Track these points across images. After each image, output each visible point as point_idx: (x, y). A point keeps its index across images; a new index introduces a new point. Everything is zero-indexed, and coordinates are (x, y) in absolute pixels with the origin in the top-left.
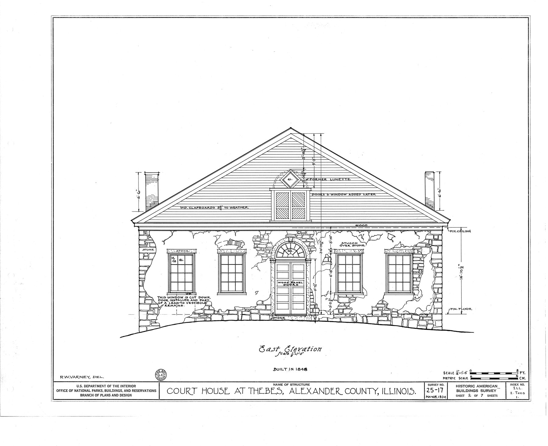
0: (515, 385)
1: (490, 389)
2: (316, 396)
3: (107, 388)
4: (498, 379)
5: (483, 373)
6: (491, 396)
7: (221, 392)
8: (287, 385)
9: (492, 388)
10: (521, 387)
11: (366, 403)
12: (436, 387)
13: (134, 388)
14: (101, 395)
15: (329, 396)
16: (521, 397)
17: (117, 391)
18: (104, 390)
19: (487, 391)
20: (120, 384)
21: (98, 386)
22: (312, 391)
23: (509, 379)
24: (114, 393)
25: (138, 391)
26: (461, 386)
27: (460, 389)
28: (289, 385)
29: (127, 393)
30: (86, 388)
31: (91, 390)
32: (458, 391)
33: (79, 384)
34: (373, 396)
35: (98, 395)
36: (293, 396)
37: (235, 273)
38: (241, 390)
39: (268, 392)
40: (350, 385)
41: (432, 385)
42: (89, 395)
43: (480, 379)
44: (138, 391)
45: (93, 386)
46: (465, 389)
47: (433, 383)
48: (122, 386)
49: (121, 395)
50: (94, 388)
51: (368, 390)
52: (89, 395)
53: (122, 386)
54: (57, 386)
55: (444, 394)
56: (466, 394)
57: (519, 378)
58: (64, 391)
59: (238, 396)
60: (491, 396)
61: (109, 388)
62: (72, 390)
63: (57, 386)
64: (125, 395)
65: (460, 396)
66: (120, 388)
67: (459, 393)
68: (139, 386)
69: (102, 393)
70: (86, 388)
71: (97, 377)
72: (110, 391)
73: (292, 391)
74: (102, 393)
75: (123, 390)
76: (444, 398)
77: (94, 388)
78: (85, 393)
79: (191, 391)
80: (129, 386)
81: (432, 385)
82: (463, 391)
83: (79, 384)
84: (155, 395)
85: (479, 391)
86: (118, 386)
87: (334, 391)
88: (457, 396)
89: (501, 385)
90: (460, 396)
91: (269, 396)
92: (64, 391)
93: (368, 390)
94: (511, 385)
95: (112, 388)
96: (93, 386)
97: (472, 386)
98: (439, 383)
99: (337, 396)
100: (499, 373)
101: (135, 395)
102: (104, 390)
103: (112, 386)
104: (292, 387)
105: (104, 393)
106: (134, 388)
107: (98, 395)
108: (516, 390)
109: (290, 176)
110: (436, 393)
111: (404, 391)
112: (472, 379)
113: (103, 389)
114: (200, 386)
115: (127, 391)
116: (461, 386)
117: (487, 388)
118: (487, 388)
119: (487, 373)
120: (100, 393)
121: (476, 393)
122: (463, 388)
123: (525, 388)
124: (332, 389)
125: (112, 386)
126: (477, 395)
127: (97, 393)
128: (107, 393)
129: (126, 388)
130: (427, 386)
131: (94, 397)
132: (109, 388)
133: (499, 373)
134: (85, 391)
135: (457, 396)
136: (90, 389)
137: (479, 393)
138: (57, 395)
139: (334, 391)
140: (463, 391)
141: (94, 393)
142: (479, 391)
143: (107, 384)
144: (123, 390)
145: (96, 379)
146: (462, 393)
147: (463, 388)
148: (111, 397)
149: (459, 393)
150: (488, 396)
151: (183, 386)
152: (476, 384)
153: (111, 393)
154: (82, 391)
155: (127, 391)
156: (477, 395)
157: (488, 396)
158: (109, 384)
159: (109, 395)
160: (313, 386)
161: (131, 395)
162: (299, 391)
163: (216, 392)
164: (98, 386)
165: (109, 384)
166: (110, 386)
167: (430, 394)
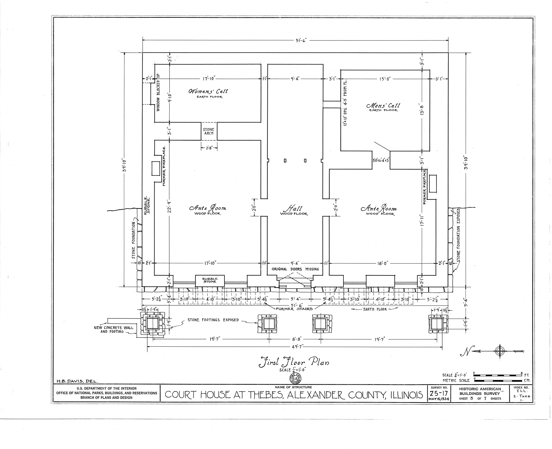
0: (519, 387)
1: (493, 391)
3: (107, 390)
4: (502, 381)
6: (495, 399)
8: (289, 387)
9: (495, 391)
10: (526, 390)
13: (135, 391)
17: (117, 393)
18: (104, 393)
19: (491, 393)
21: (99, 388)
22: (312, 395)
24: (115, 395)
25: (139, 393)
26: (465, 389)
27: (463, 391)
28: (291, 387)
29: (128, 395)
30: (87, 391)
31: (91, 393)
32: (461, 394)
33: (80, 386)
35: (98, 397)
38: (240, 394)
39: (268, 396)
41: (435, 387)
42: (89, 397)
44: (139, 393)
45: (94, 388)
48: (123, 388)
49: (122, 398)
50: (94, 391)
51: (375, 393)
52: (89, 397)
53: (123, 388)
58: (64, 393)
60: (495, 399)
61: (110, 391)
62: (72, 393)
63: (58, 388)
64: (126, 398)
65: (463, 399)
66: (120, 391)
67: (462, 396)
68: (140, 389)
69: (102, 395)
70: (87, 391)
72: (110, 393)
73: (290, 395)
74: (102, 395)
75: (124, 393)
76: (447, 401)
77: (94, 391)
78: (85, 395)
79: (191, 396)
80: (130, 388)
81: (435, 387)
82: (466, 394)
84: (156, 398)
85: (483, 393)
86: (118, 388)
87: (336, 395)
88: (460, 399)
89: (505, 388)
90: (463, 399)
92: (64, 393)
93: (375, 393)
95: (112, 390)
96: (94, 388)
97: (476, 389)
101: (136, 398)
102: (104, 393)
103: (113, 388)
105: (104, 396)
106: (135, 391)
107: (98, 397)
112: (475, 381)
113: (104, 391)
116: (465, 389)
118: (472, 391)
120: (100, 395)
121: (479, 396)
123: (529, 391)
125: (113, 388)
126: (480, 398)
127: (98, 395)
128: (107, 395)
129: (127, 391)
130: (430, 389)
131: (95, 400)
132: (110, 391)
134: (85, 393)
135: (460, 399)
136: (91, 391)
137: (483, 396)
139: (336, 395)
140: (466, 394)
141: (95, 395)
142: (483, 393)
143: (108, 386)
144: (124, 393)
148: (112, 400)
149: (462, 396)
150: (492, 399)
152: (479, 387)
153: (112, 396)
154: (83, 393)
156: (480, 398)
157: (492, 399)
158: (110, 386)
159: (109, 398)
161: (131, 398)
162: (298, 395)
164: (99, 388)
165: (110, 386)
166: (110, 388)
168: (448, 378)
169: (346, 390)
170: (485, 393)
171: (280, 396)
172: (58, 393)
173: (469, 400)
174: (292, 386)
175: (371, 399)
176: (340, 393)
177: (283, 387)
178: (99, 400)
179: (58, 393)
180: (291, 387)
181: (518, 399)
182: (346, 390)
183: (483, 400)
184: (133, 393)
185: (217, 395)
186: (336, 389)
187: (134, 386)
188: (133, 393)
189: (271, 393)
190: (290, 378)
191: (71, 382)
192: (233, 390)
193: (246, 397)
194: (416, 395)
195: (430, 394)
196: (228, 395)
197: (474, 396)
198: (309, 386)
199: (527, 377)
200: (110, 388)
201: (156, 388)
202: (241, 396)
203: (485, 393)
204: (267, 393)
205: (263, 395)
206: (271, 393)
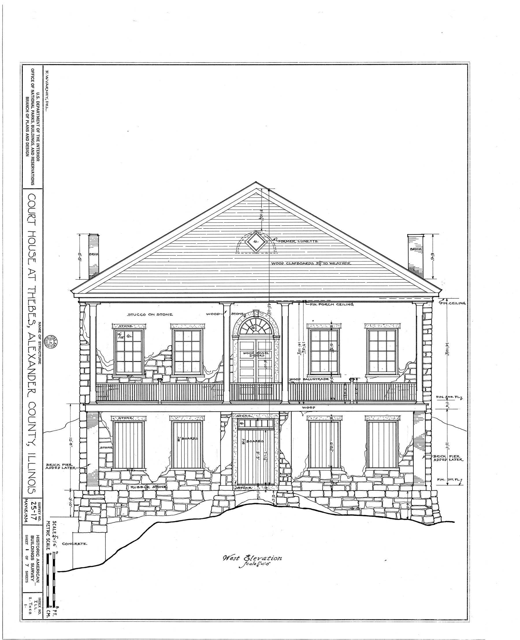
0: (40, 604)
1: (35, 574)
2: (26, 364)
3: (36, 127)
4: (48, 563)
5: (54, 588)
6: (27, 575)
7: (31, 255)
8: (40, 338)
9: (35, 576)
10: (37, 610)
11: (19, 416)
12: (37, 512)
13: (35, 159)
14: (28, 121)
15: (26, 380)
16: (26, 610)
17: (33, 139)
18: (33, 124)
19: (33, 571)
20: (41, 143)
21: (38, 117)
22: (32, 359)
23: (48, 576)
24: (30, 136)
25: (33, 164)
26: (38, 541)
27: (35, 539)
28: (40, 340)
29: (30, 151)
30: (35, 104)
31: (33, 109)
32: (32, 537)
33: (41, 95)
34: (27, 439)
35: (28, 117)
36: (26, 337)
37: (192, 341)
38: (32, 275)
39: (31, 309)
40: (39, 409)
41: (40, 507)
42: (27, 106)
43: (48, 584)
44: (33, 164)
45: (38, 112)
46: (35, 545)
47: (41, 507)
48: (38, 145)
49: (27, 145)
50: (35, 112)
51: (33, 433)
52: (27, 106)
53: (38, 145)
54: (38, 70)
55: (30, 521)
56: (29, 547)
57: (48, 609)
58: (33, 77)
59: (26, 272)
60: (27, 575)
61: (35, 130)
62: (33, 87)
63: (38, 70)
64: (27, 149)
65: (27, 539)
66: (36, 143)
67: (29, 538)
68: (38, 165)
69: (30, 122)
70: (35, 104)
71: (47, 105)
72: (33, 131)
73: (31, 336)
74: (30, 122)
75: (33, 146)
76: (24, 520)
77: (35, 112)
78: (30, 102)
79: (31, 219)
80: (38, 153)
81: (40, 507)
82: (32, 543)
83: (41, 95)
84: (27, 184)
85: (33, 562)
86: (38, 140)
87: (32, 386)
88: (27, 536)
89: (38, 587)
90: (27, 539)
91: (26, 311)
92: (33, 77)
93: (33, 433)
94: (40, 600)
95: (36, 133)
96: (38, 112)
97: (38, 554)
98: (41, 516)
99: (26, 391)
100: (54, 565)
101: (27, 160)
102: (33, 124)
103: (38, 134)
104: (37, 337)
105: (30, 124)
106: (35, 159)
107: (28, 117)
108: (34, 604)
109: (256, 238)
110: (30, 512)
111: (32, 483)
112: (48, 555)
113: (35, 124)
114: (38, 229)
115: (33, 151)
116: (38, 541)
117: (35, 570)
118: (35, 570)
119: (54, 592)
120: (30, 119)
121: (30, 558)
122: (35, 542)
123: (35, 615)
124: (34, 314)
125: (38, 134)
126: (27, 559)
127: (30, 116)
128: (30, 127)
129: (35, 150)
130: (38, 501)
131: (25, 113)
132: (35, 130)
133: (54, 565)
134: (33, 102)
135: (27, 536)
136: (35, 109)
137: (30, 562)
138: (27, 70)
139: (32, 386)
140: (32, 543)
141: (30, 113)
142: (33, 562)
143: (41, 128)
144: (33, 146)
145: (45, 103)
146: (30, 542)
147: (35, 542)
148: (25, 133)
149: (29, 538)
150: (27, 572)
151: (38, 211)
152: (40, 558)
153: (29, 133)
154: (33, 99)
155: (33, 151)
156: (27, 559)
157: (27, 572)
158: (41, 131)
159: (27, 130)
160: (38, 367)
161: (27, 155)
162: (31, 344)
163: (31, 248)
164: (38, 117)
165: (41, 131)
166: (38, 131)
167: (29, 506)
168: (51, 527)
169: (36, 397)
170: (33, 565)
171: (31, 322)
172: (33, 71)
173: (25, 547)
174: (41, 341)
175: (26, 427)
176: (34, 391)
177: (40, 331)
178: (25, 119)
179: (33, 71)
180: (40, 340)
181: (26, 601)
182: (36, 397)
183: (25, 562)
184: (33, 158)
185: (31, 248)
186: (38, 387)
187: (41, 158)
188: (33, 158)
189: (34, 312)
190: (52, 336)
191: (45, 87)
192: (37, 266)
193: (29, 283)
194: (32, 486)
195: (34, 501)
196: (31, 261)
197: (30, 552)
198: (41, 361)
199: (52, 613)
200: (38, 131)
201: (38, 184)
202: (31, 276)
203: (33, 565)
204: (34, 308)
205: (32, 303)
206: (34, 312)
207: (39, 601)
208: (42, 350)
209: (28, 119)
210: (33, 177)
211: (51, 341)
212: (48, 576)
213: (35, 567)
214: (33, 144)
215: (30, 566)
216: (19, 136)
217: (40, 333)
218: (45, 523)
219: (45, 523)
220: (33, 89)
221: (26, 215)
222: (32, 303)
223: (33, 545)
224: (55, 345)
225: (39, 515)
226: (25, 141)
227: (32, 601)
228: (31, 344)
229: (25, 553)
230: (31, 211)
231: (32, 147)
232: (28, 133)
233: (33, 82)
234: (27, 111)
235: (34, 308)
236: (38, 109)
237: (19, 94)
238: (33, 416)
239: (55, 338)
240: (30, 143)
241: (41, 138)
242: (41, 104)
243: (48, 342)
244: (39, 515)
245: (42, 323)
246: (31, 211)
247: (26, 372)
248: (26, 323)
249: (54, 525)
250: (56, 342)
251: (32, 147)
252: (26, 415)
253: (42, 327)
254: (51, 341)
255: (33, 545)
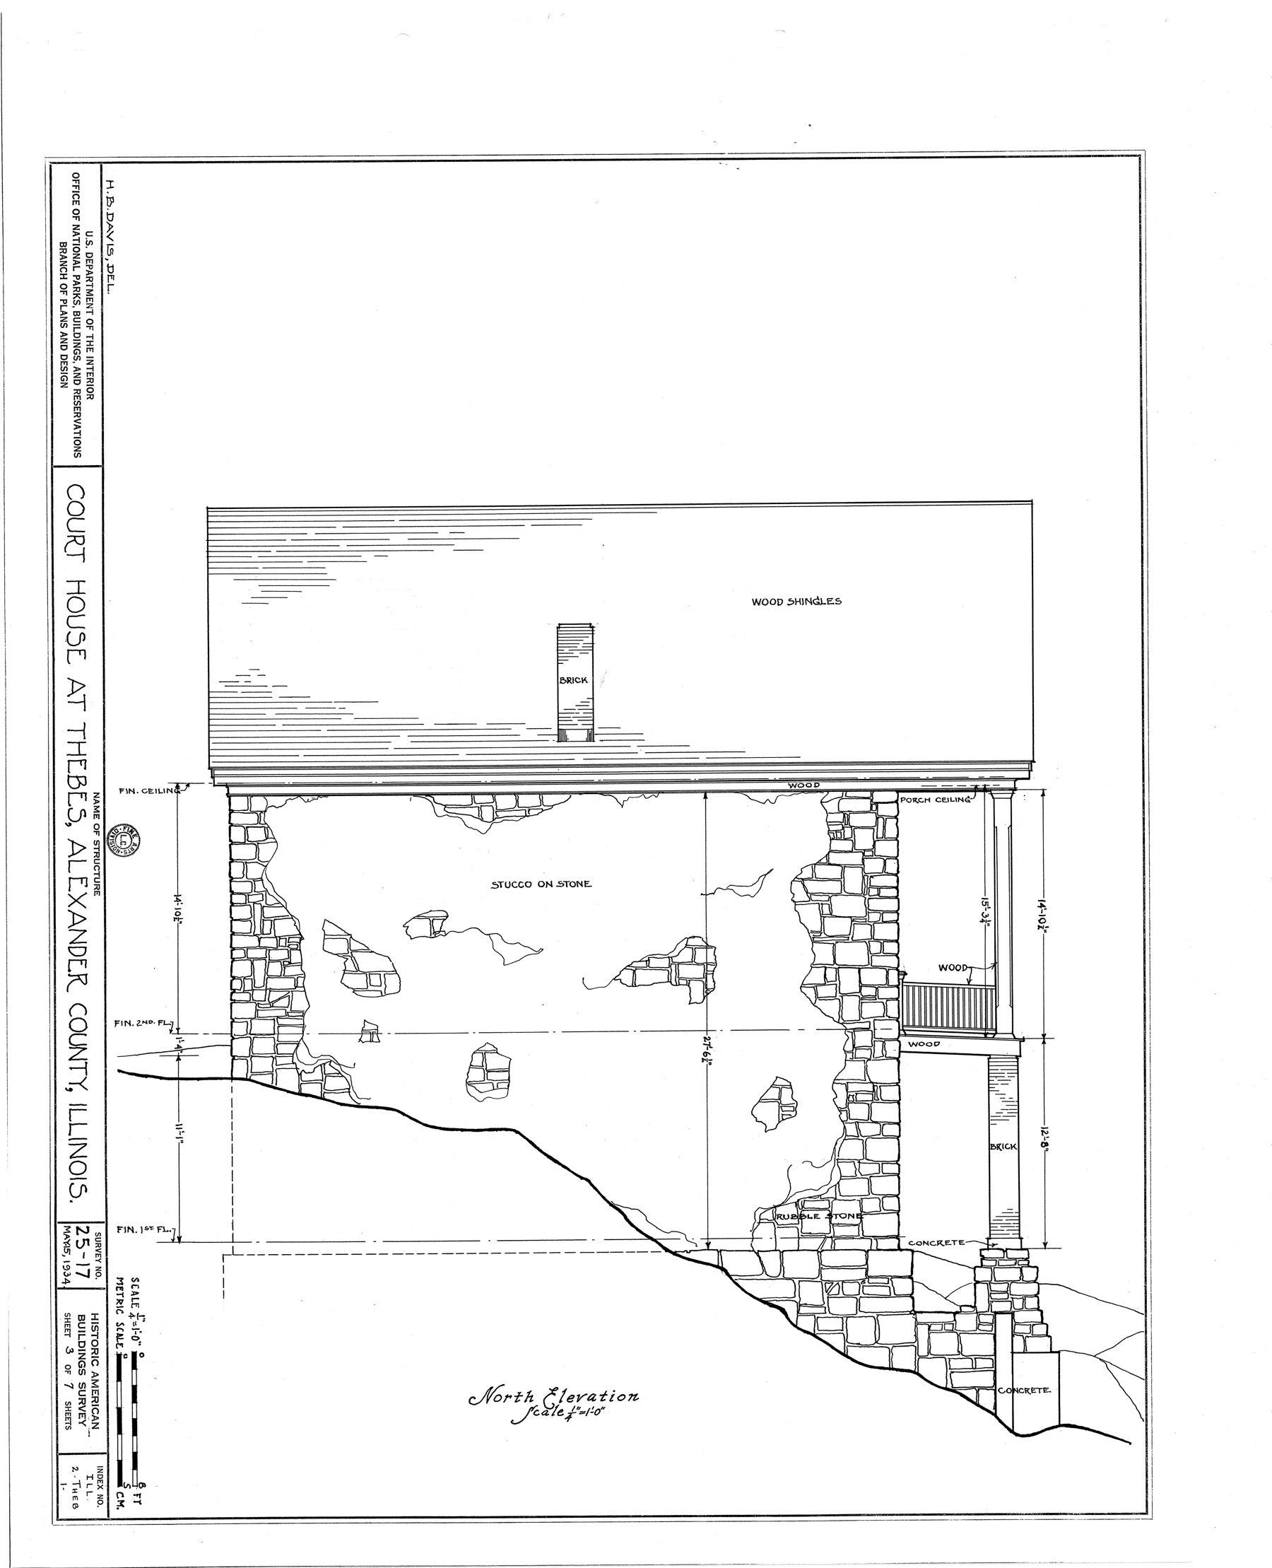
1: (88, 1408)
3: (84, 317)
4: (120, 1431)
5: (134, 1388)
6: (68, 1413)
8: (97, 832)
9: (89, 1414)
10: (93, 1498)
11: (46, 1057)
13: (84, 394)
14: (65, 301)
16: (66, 1495)
17: (77, 346)
18: (77, 308)
19: (83, 1401)
21: (89, 292)
23: (120, 1463)
24: (70, 338)
25: (77, 406)
26: (95, 1328)
27: (88, 1324)
28: (96, 838)
29: (71, 375)
30: (83, 258)
31: (77, 271)
32: (82, 1318)
33: (96, 239)
35: (64, 291)
36: (64, 850)
38: (78, 697)
41: (99, 1245)
42: (63, 265)
44: (77, 406)
45: (90, 279)
48: (90, 361)
49: (64, 360)
50: (83, 280)
52: (63, 265)
53: (90, 361)
54: (89, 175)
56: (73, 1342)
58: (76, 193)
59: (63, 687)
60: (68, 1413)
61: (83, 324)
62: (77, 217)
63: (89, 175)
64: (64, 370)
65: (68, 1324)
66: (84, 354)
67: (74, 1322)
68: (90, 408)
69: (70, 303)
72: (77, 325)
73: (76, 847)
74: (70, 303)
75: (78, 364)
77: (83, 280)
78: (70, 254)
79: (73, 548)
80: (91, 380)
81: (99, 1245)
84: (64, 454)
85: (82, 1379)
87: (77, 968)
88: (67, 1316)
90: (68, 1324)
91: (62, 789)
92: (76, 193)
93: (82, 1064)
94: (100, 1470)
95: (84, 331)
96: (90, 279)
97: (95, 1359)
98: (103, 1265)
99: (63, 979)
100: (135, 1433)
101: (64, 398)
102: (77, 308)
103: (90, 332)
105: (69, 309)
106: (84, 394)
107: (64, 291)
108: (84, 1483)
112: (119, 1356)
113: (82, 308)
114: (90, 571)
116: (95, 1328)
117: (89, 1399)
118: (89, 1399)
119: (134, 1400)
120: (70, 297)
121: (75, 1369)
122: (89, 1332)
123: (89, 1507)
125: (90, 332)
126: (68, 1371)
127: (70, 290)
128: (70, 317)
129: (83, 372)
132: (83, 324)
134: (77, 255)
135: (67, 1316)
136: (82, 271)
137: (75, 1378)
138: (63, 176)
139: (77, 968)
141: (70, 282)
142: (82, 1379)
143: (96, 318)
144: (78, 364)
146: (75, 1330)
147: (89, 1332)
149: (74, 1322)
150: (68, 1404)
151: (90, 525)
152: (101, 1369)
153: (69, 331)
156: (68, 1371)
157: (68, 1404)
158: (97, 325)
160: (93, 903)
161: (64, 385)
162: (78, 870)
163: (73, 622)
164: (89, 292)
165: (97, 325)
166: (90, 326)
170: (82, 1386)
172: (76, 177)
173: (64, 1342)
174: (101, 838)
178: (58, 296)
179: (76, 177)
180: (96, 838)
184: (78, 391)
187: (97, 393)
190: (125, 826)
191: (106, 221)
193: (69, 716)
194: (78, 1176)
197: (75, 1356)
198: (101, 889)
200: (90, 326)
201: (91, 454)
202: (72, 698)
204: (82, 780)
205: (77, 769)
207: (101, 1476)
208: (101, 861)
209: (64, 297)
210: (77, 439)
211: (124, 839)
212: (120, 1463)
213: (88, 1393)
214: (77, 303)
215: (77, 1389)
216: (43, 327)
217: (97, 821)
218: (113, 1283)
219: (113, 1283)
220: (77, 222)
221: (61, 536)
222: (77, 769)
223: (82, 1338)
224: (134, 849)
225: (98, 1264)
226: (58, 352)
227: (81, 1476)
228: (78, 870)
229: (64, 1359)
230: (75, 525)
231: (76, 364)
232: (64, 330)
233: (76, 206)
234: (64, 276)
235: (82, 780)
236: (90, 273)
237: (42, 234)
238: (78, 614)
239: (132, 831)
240: (71, 356)
241: (97, 344)
242: (97, 258)
243: (118, 840)
244: (98, 1264)
245: (101, 795)
246: (77, 1040)
247: (65, 937)
248: (62, 818)
249: (135, 1289)
250: (136, 840)
251: (76, 364)
252: (61, 517)
253: (101, 804)
254: (124, 839)
255: (82, 1338)
